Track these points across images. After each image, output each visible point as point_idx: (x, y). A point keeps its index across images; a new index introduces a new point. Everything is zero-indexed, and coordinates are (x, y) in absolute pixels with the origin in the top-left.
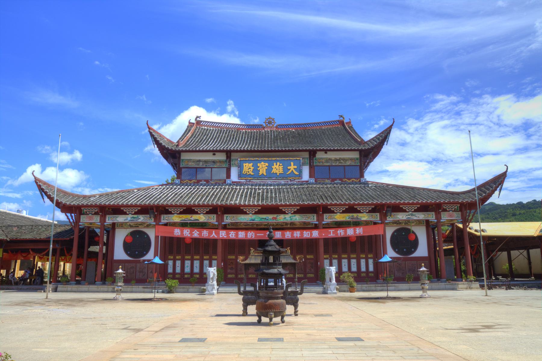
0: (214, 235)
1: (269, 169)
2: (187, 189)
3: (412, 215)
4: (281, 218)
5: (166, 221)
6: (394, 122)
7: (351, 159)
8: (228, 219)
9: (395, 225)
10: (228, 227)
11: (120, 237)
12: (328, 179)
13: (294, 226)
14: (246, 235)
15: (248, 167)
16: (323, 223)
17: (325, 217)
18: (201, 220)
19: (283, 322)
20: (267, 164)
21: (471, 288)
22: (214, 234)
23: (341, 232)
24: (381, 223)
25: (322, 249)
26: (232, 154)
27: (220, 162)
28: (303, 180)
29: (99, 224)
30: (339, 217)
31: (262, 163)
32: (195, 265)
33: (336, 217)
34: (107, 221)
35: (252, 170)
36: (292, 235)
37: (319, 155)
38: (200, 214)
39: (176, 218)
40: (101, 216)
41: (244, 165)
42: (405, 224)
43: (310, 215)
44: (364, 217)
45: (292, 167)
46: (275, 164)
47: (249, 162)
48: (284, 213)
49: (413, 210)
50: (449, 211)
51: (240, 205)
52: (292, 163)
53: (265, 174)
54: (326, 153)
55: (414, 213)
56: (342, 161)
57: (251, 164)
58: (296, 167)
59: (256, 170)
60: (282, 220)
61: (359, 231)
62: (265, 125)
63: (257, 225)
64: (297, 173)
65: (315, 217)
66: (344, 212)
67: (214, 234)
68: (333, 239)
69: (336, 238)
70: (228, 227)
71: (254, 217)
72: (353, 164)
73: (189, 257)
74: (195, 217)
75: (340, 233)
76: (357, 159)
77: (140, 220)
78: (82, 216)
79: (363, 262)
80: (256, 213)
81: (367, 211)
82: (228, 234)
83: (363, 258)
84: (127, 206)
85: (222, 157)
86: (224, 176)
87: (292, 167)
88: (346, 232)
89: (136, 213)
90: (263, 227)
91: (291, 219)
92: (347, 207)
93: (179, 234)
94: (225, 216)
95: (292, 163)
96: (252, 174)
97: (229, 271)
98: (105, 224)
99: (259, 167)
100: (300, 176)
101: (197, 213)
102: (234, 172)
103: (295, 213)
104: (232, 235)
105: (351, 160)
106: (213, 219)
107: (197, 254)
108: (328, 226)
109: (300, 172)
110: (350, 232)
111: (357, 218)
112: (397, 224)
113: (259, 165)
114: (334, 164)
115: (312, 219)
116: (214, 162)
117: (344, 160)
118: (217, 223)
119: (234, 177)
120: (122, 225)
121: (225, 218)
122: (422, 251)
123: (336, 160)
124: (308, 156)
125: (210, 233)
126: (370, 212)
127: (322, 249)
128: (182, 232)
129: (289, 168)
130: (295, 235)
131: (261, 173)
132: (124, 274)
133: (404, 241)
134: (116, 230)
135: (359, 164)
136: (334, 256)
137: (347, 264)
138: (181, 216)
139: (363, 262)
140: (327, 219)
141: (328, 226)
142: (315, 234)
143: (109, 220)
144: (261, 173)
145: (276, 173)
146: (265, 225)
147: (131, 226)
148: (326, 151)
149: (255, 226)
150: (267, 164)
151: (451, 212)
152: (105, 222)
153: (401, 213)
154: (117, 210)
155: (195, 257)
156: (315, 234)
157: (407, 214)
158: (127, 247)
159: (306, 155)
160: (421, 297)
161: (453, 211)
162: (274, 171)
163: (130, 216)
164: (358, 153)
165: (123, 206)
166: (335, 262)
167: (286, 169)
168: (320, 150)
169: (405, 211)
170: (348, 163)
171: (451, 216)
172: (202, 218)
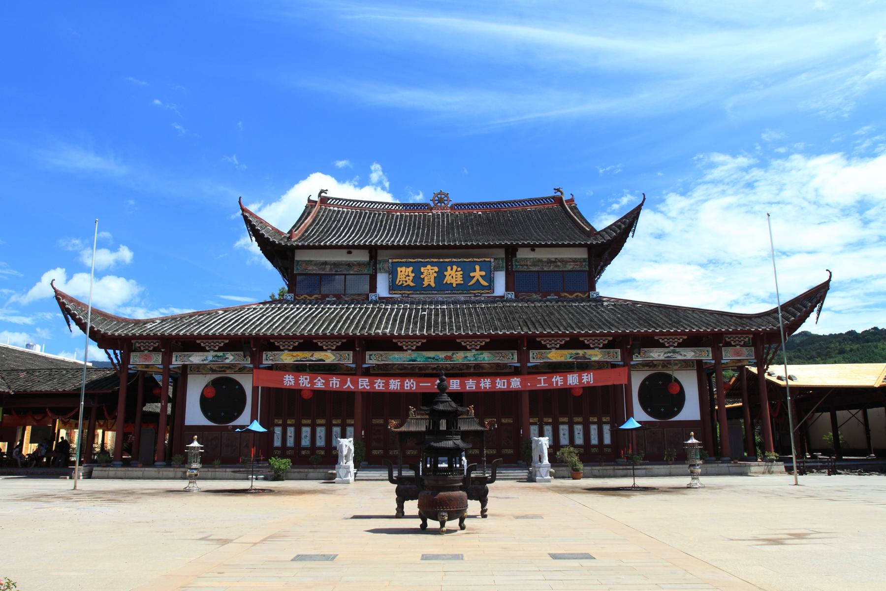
0: (349, 385)
1: (440, 276)
3: (674, 352)
5: (270, 362)
6: (644, 199)
7: (574, 261)
8: (373, 359)
9: (646, 368)
11: (195, 389)
13: (481, 371)
15: (405, 274)
16: (529, 365)
17: (531, 355)
18: (328, 361)
20: (436, 269)
21: (770, 472)
23: (557, 381)
24: (624, 366)
25: (526, 408)
26: (379, 252)
28: (495, 295)
29: (161, 367)
30: (555, 356)
31: (429, 267)
32: (318, 435)
33: (549, 356)
34: (368, 361)
35: (411, 278)
36: (478, 384)
37: (522, 254)
38: (593, 348)
39: (287, 358)
41: (399, 269)
42: (663, 367)
43: (507, 352)
44: (596, 355)
45: (478, 274)
46: (449, 268)
47: (407, 264)
48: (464, 349)
52: (477, 267)
53: (433, 285)
54: (533, 250)
55: (678, 349)
57: (411, 268)
58: (483, 273)
59: (418, 278)
60: (460, 361)
61: (588, 378)
62: (432, 205)
63: (420, 368)
64: (485, 283)
65: (516, 356)
66: (562, 347)
71: (414, 355)
72: (577, 268)
73: (566, 420)
74: (318, 355)
75: (557, 382)
76: (584, 260)
77: (227, 361)
78: (132, 355)
79: (594, 429)
80: (418, 349)
82: (372, 384)
83: (594, 423)
84: (207, 337)
85: (362, 257)
87: (478, 274)
88: (565, 380)
90: (430, 371)
91: (476, 360)
93: (293, 383)
95: (477, 267)
96: (412, 284)
98: (171, 367)
99: (422, 273)
100: (491, 287)
101: (321, 349)
103: (483, 348)
105: (574, 261)
106: (347, 359)
108: (538, 370)
109: (490, 280)
110: (572, 379)
111: (584, 357)
112: (650, 367)
113: (422, 269)
114: (545, 269)
115: (511, 358)
119: (382, 289)
120: (198, 369)
121: (367, 357)
122: (691, 411)
123: (550, 262)
124: (504, 256)
126: (605, 347)
127: (526, 408)
128: (297, 380)
129: (472, 274)
130: (482, 385)
131: (426, 283)
133: (662, 395)
135: (587, 268)
136: (545, 420)
138: (295, 353)
139: (594, 429)
140: (535, 358)
141: (538, 370)
142: (516, 383)
143: (177, 361)
144: (426, 283)
145: (451, 284)
147: (213, 371)
148: (533, 248)
149: (417, 371)
150: (436, 269)
151: (738, 347)
153: (656, 349)
154: (191, 344)
156: (516, 383)
157: (666, 350)
159: (501, 254)
161: (741, 346)
163: (212, 353)
166: (548, 429)
167: (467, 277)
168: (524, 246)
169: (662, 346)
170: (569, 267)
171: (738, 354)
172: (329, 357)
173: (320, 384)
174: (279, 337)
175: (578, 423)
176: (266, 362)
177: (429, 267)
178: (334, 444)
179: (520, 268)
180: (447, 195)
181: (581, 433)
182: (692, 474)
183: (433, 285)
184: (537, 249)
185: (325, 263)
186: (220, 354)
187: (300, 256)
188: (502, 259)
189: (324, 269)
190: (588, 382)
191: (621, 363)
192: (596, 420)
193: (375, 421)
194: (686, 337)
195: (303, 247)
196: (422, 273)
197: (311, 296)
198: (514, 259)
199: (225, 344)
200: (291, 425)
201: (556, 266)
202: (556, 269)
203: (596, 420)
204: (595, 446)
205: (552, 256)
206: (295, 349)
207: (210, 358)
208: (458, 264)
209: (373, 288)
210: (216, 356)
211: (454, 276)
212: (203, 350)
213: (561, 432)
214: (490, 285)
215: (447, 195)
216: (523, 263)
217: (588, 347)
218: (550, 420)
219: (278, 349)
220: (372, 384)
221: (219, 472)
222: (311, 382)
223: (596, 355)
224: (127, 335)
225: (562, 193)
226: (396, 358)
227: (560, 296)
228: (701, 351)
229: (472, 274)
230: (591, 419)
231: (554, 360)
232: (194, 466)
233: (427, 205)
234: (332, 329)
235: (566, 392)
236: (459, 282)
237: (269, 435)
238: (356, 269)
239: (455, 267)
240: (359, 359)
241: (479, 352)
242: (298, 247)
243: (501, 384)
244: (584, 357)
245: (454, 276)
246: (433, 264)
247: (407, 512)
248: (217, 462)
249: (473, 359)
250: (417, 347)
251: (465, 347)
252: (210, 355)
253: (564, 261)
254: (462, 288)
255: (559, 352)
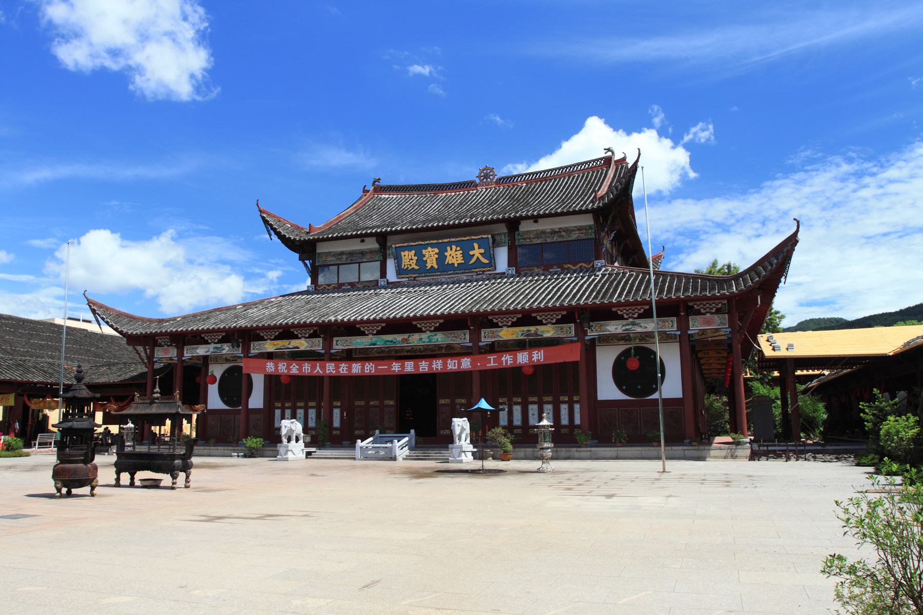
0: (318, 370)
1: (441, 258)
2: (570, 279)
3: (633, 324)
4: (415, 340)
5: (257, 351)
6: (639, 154)
7: (580, 229)
8: (340, 344)
9: (622, 342)
10: (354, 356)
11: (606, 360)
12: (538, 267)
13: (452, 351)
14: (363, 369)
15: (409, 258)
16: (481, 344)
17: (483, 334)
18: (302, 348)
19: (93, 495)
20: (437, 250)
21: (734, 457)
22: (318, 368)
23: (507, 359)
24: (577, 341)
25: (476, 388)
26: (389, 238)
27: (371, 252)
28: (497, 271)
29: (729, 330)
30: (507, 334)
31: (429, 249)
32: (310, 416)
33: (500, 334)
34: (335, 347)
35: (415, 261)
36: (430, 366)
37: (525, 227)
38: (545, 324)
39: (269, 346)
40: (324, 339)
41: (403, 254)
42: (640, 340)
43: (459, 332)
44: (548, 331)
45: (477, 252)
46: (449, 248)
47: (409, 248)
48: (420, 331)
49: (636, 316)
50: (704, 314)
51: (612, 305)
52: (476, 246)
53: (436, 267)
54: (536, 222)
55: (637, 321)
56: (563, 234)
57: (413, 252)
58: (482, 251)
59: (421, 261)
60: (416, 343)
61: (538, 356)
62: (478, 181)
63: (396, 351)
64: (485, 261)
65: (468, 336)
66: (514, 325)
67: (318, 368)
68: (493, 371)
69: (500, 369)
70: (354, 356)
71: (375, 339)
72: (583, 236)
73: (535, 399)
74: (294, 343)
75: (506, 361)
76: (590, 227)
77: (224, 352)
78: (156, 349)
79: (564, 409)
80: (379, 333)
81: (554, 321)
82: (337, 367)
83: (564, 402)
84: (500, 313)
85: (372, 244)
86: (376, 275)
87: (477, 252)
88: (515, 359)
89: (220, 342)
90: (406, 354)
91: (430, 341)
92: (520, 316)
93: (273, 370)
94: (335, 339)
95: (476, 246)
96: (417, 268)
97: (356, 425)
98: (481, 344)
99: (424, 256)
100: (492, 264)
101: (296, 337)
102: (391, 265)
103: (437, 329)
104: (343, 369)
105: (579, 230)
106: (317, 345)
107: (288, 400)
108: (493, 348)
109: (492, 258)
110: (522, 358)
111: (536, 334)
112: (626, 340)
113: (424, 251)
114: (549, 240)
115: (463, 338)
116: (363, 253)
117: (567, 230)
118: (323, 352)
119: (392, 276)
120: (608, 340)
121: (334, 342)
122: (672, 386)
123: (553, 232)
124: (506, 231)
125: (313, 368)
126: (558, 322)
127: (476, 388)
128: (276, 367)
129: (471, 253)
130: (434, 366)
131: (429, 266)
132: (551, 427)
133: (638, 371)
134: (597, 348)
135: (593, 236)
136: (515, 399)
137: (536, 413)
138: (276, 342)
139: (564, 409)
140: (487, 337)
141: (493, 348)
142: (466, 363)
143: (189, 353)
144: (429, 266)
145: (453, 264)
146: (409, 351)
147: (227, 360)
148: (536, 218)
149: (393, 354)
150: (437, 250)
151: (708, 315)
152: (183, 356)
153: (613, 322)
154: (197, 338)
155: (546, 399)
156: (466, 363)
157: (625, 322)
158: (620, 375)
159: (503, 229)
160: (538, 471)
161: (712, 313)
162: (449, 260)
163: (213, 345)
164: (590, 216)
165: (493, 313)
166: (548, 408)
167: (467, 256)
168: (527, 218)
169: (621, 318)
170: (574, 236)
171: (708, 323)
172: (303, 344)
173: (294, 370)
174: (539, 310)
175: (548, 403)
176: (254, 351)
177: (429, 249)
178: (276, 425)
179: (522, 242)
180: (492, 170)
181: (530, 415)
182: (541, 458)
183: (436, 267)
184: (540, 220)
185: (342, 253)
186: (219, 345)
187: (321, 248)
188: (504, 234)
189: (340, 259)
190: (538, 360)
191: (575, 339)
192: (566, 399)
193: (357, 403)
194: (565, 313)
195: (323, 240)
196: (424, 256)
197: (575, 265)
198: (517, 233)
199: (383, 328)
200: (288, 408)
201: (560, 236)
202: (560, 240)
203: (566, 399)
204: (565, 426)
205: (556, 227)
206: (276, 338)
207: (211, 350)
208: (457, 244)
209: (383, 274)
210: (216, 348)
211: (454, 256)
212: (206, 343)
213: (531, 412)
214: (491, 262)
215: (492, 170)
216: (526, 236)
217: (540, 323)
218: (520, 400)
219: (496, 326)
220: (337, 367)
221: (213, 450)
222: (288, 368)
223: (548, 331)
224: (198, 329)
225: (613, 153)
226: (359, 342)
227: (563, 269)
228: (664, 321)
229: (471, 253)
230: (562, 398)
231: (505, 338)
232: (546, 445)
233: (472, 182)
234: (578, 300)
235: (517, 370)
236: (460, 262)
237: (495, 414)
238: (368, 256)
239: (454, 247)
240: (328, 344)
241: (433, 334)
242: (319, 240)
243: (452, 365)
244: (536, 334)
245: (454, 256)
246: (433, 246)
247: (122, 483)
248: (212, 441)
249: (427, 340)
250: (557, 320)
251: (541, 321)
252: (211, 347)
253: (568, 231)
254: (464, 267)
255: (511, 329)
